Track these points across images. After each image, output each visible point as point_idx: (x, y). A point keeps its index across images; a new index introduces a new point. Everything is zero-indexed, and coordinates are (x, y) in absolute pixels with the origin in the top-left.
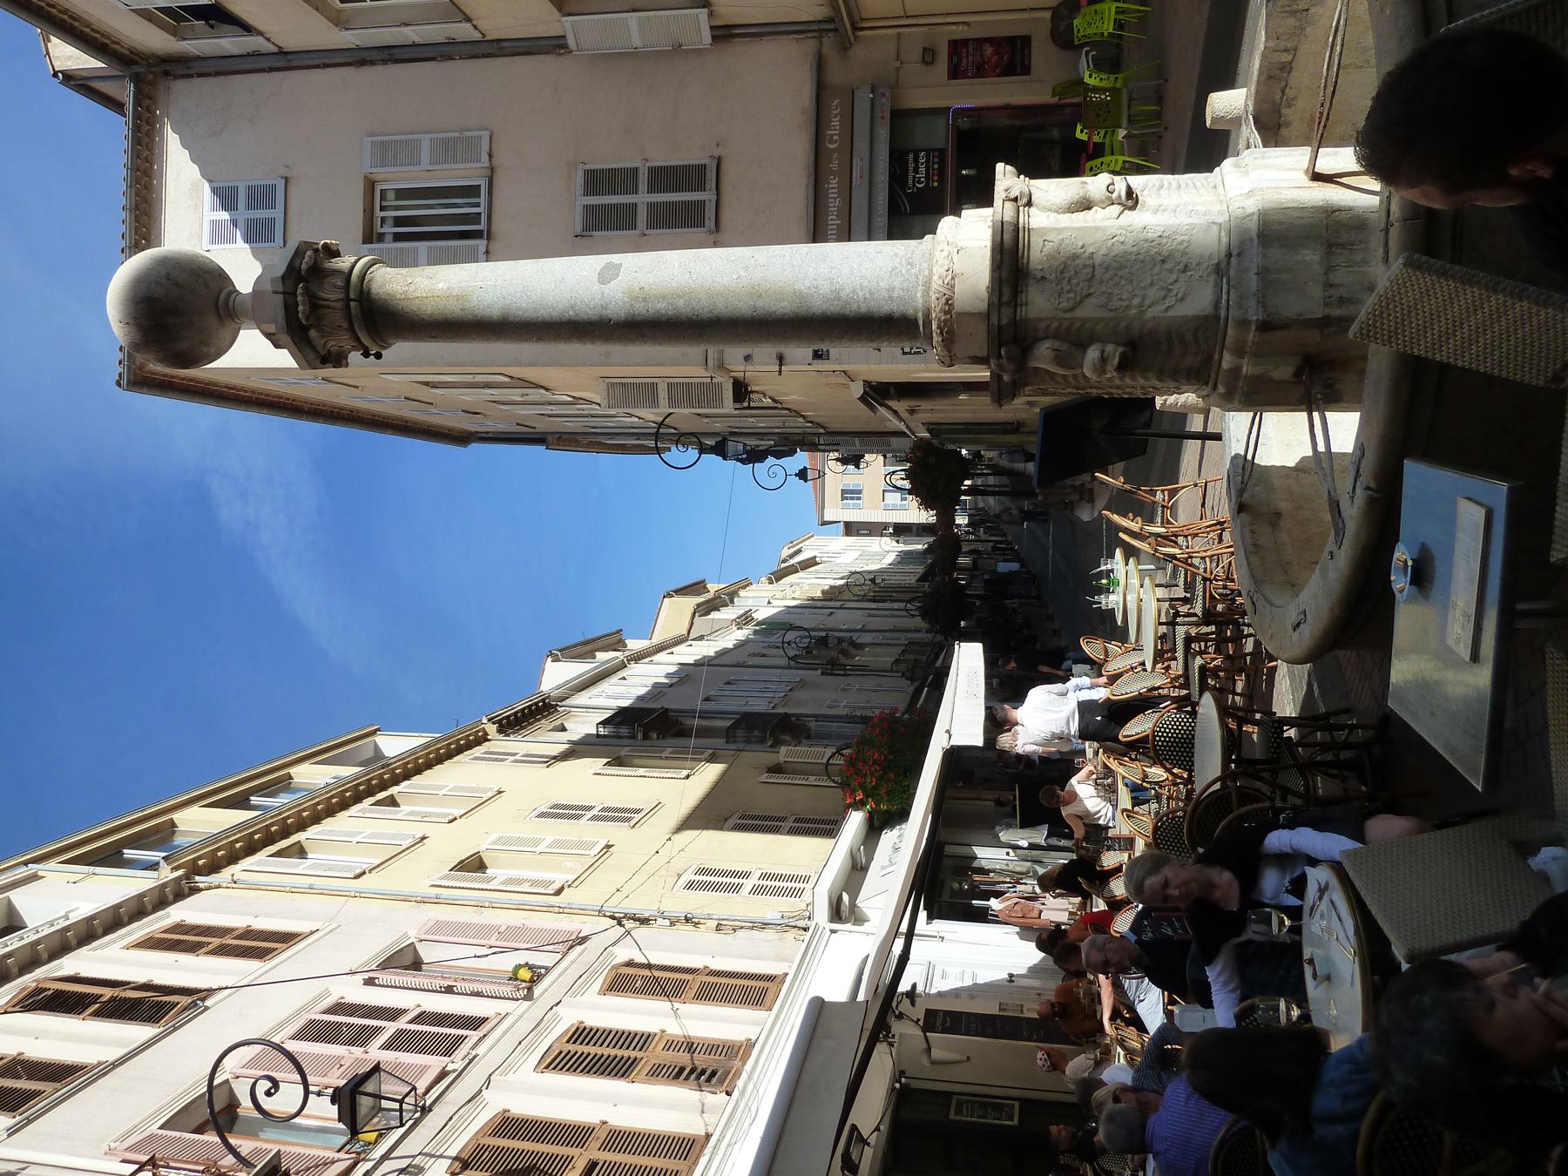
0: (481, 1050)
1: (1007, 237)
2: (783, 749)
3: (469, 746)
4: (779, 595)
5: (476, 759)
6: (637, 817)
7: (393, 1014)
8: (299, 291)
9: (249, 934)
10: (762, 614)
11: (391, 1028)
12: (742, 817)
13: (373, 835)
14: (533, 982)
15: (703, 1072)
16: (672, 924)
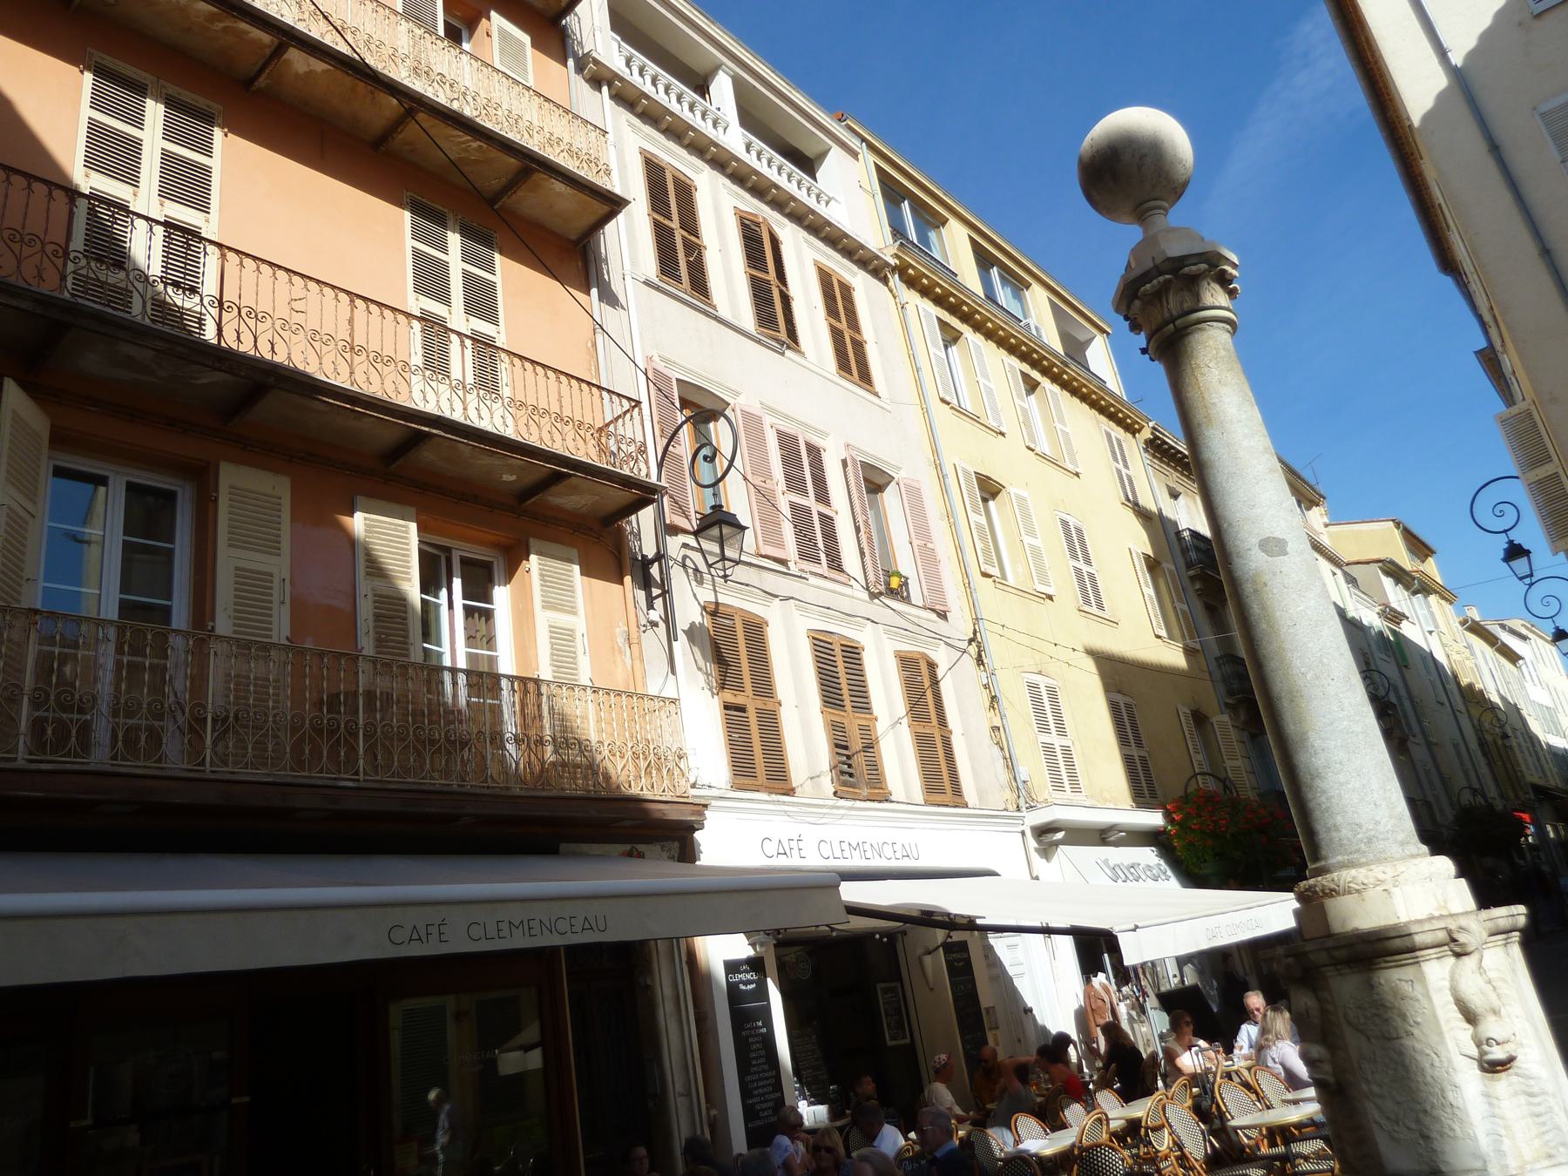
0: (813, 580)
1: (1398, 943)
2: (1225, 718)
3: (1120, 423)
4: (1447, 639)
5: (1109, 436)
6: (1094, 610)
7: (823, 496)
8: (1161, 279)
9: (859, 346)
10: (1407, 629)
11: (810, 501)
12: (1128, 706)
13: (989, 391)
14: (892, 593)
15: (850, 766)
16: (986, 686)
